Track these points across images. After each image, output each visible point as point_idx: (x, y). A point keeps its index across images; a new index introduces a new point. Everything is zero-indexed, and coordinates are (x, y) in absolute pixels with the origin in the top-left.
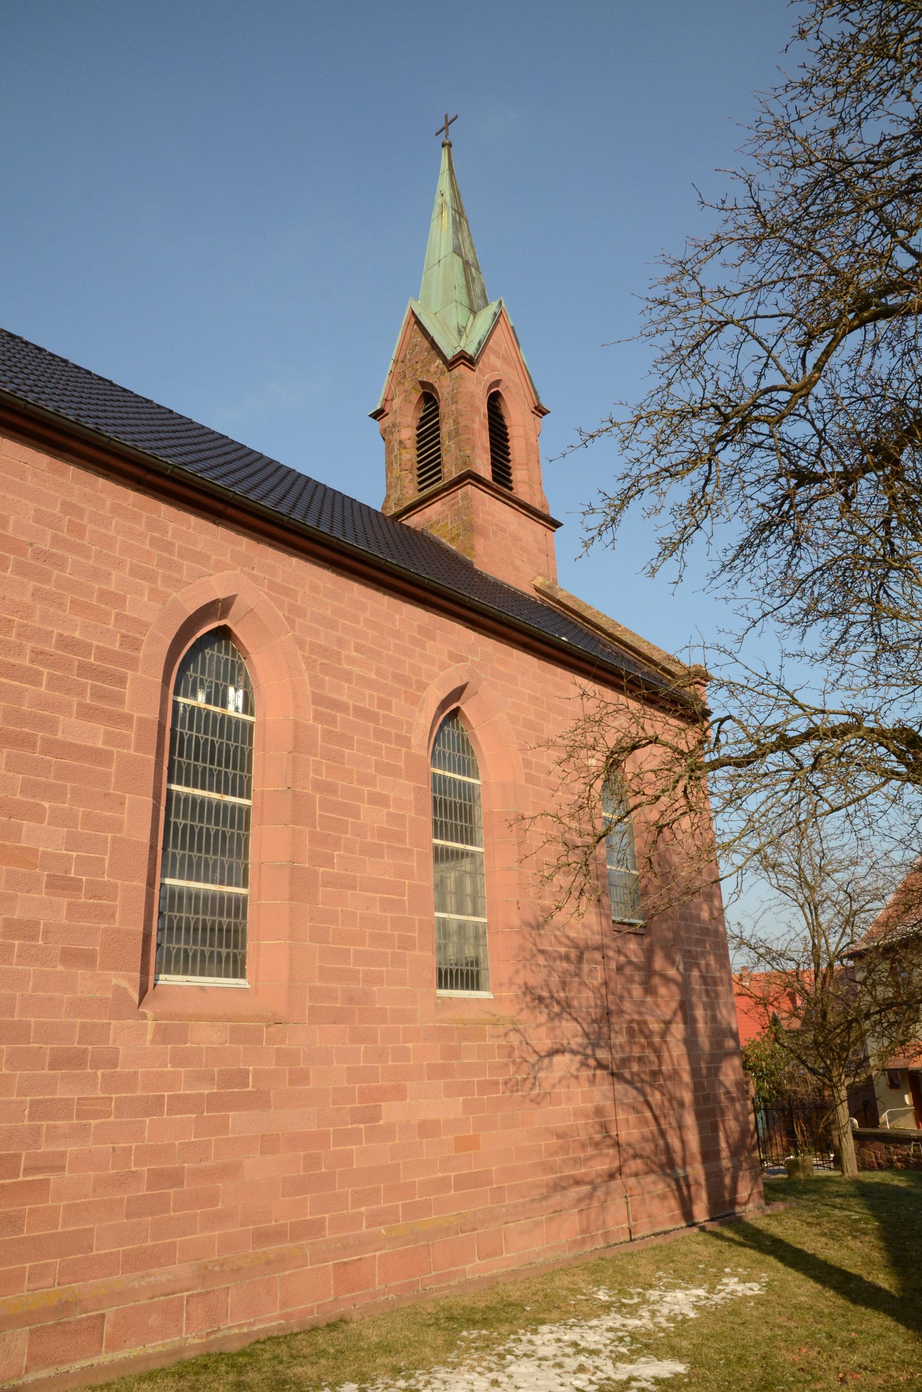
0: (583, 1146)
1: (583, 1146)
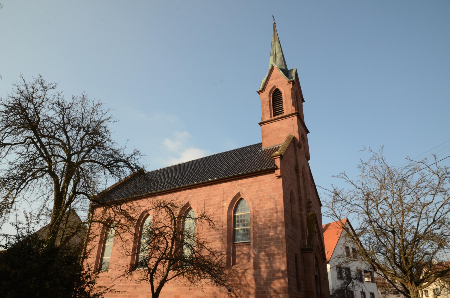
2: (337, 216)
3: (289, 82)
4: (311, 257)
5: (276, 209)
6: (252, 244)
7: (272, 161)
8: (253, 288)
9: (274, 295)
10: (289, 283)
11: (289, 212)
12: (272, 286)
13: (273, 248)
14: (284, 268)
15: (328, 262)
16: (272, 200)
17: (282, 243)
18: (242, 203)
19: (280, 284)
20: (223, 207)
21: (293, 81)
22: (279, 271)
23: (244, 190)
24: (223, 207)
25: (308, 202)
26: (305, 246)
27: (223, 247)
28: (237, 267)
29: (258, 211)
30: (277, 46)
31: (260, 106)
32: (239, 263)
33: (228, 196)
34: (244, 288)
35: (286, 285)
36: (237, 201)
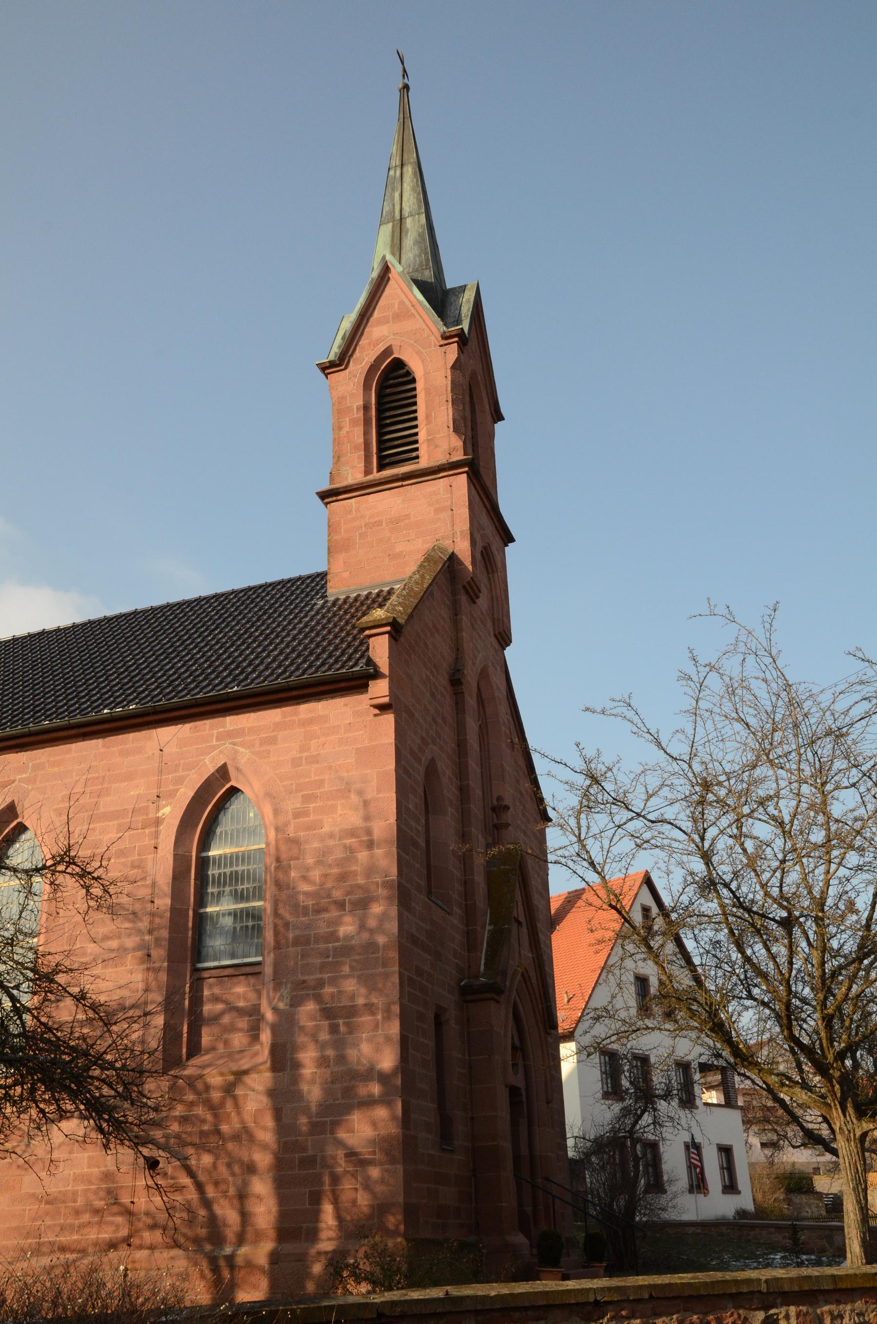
0: (77, 1213)
1: (77, 1213)
2: (592, 864)
3: (445, 337)
4: (498, 1018)
5: (369, 832)
6: (268, 970)
7: (361, 643)
8: (265, 1147)
9: (346, 1172)
10: (406, 1121)
11: (415, 844)
12: (342, 1135)
13: (350, 985)
14: (388, 1061)
15: (569, 1036)
16: (354, 798)
17: (384, 965)
18: (235, 806)
19: (374, 1124)
20: (158, 822)
21: (461, 334)
22: (371, 1073)
23: (244, 756)
24: (158, 822)
25: (494, 809)
26: (477, 977)
27: (153, 984)
28: (203, 1067)
29: (295, 842)
30: (407, 187)
31: (328, 423)
32: (213, 1049)
33: (180, 781)
34: (230, 1146)
35: (394, 1129)
36: (215, 798)
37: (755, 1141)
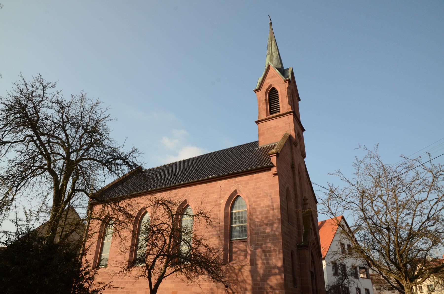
2: (332, 213)
3: (285, 81)
4: (307, 254)
5: (273, 206)
6: (249, 241)
7: (269, 158)
8: (249, 284)
9: (270, 291)
10: (285, 279)
11: (285, 209)
12: (269, 282)
13: (269, 245)
14: (280, 264)
15: (324, 259)
16: (269, 198)
17: (278, 240)
18: (239, 200)
19: (277, 280)
20: (220, 204)
21: (289, 80)
22: (275, 267)
23: (241, 187)
24: (220, 204)
25: (303, 200)
26: (301, 243)
27: (220, 243)
28: (233, 264)
29: (254, 209)
30: (273, 46)
31: (257, 104)
32: (236, 260)
33: (225, 194)
34: (241, 284)
35: (282, 281)
36: (234, 198)
37: (374, 288)
